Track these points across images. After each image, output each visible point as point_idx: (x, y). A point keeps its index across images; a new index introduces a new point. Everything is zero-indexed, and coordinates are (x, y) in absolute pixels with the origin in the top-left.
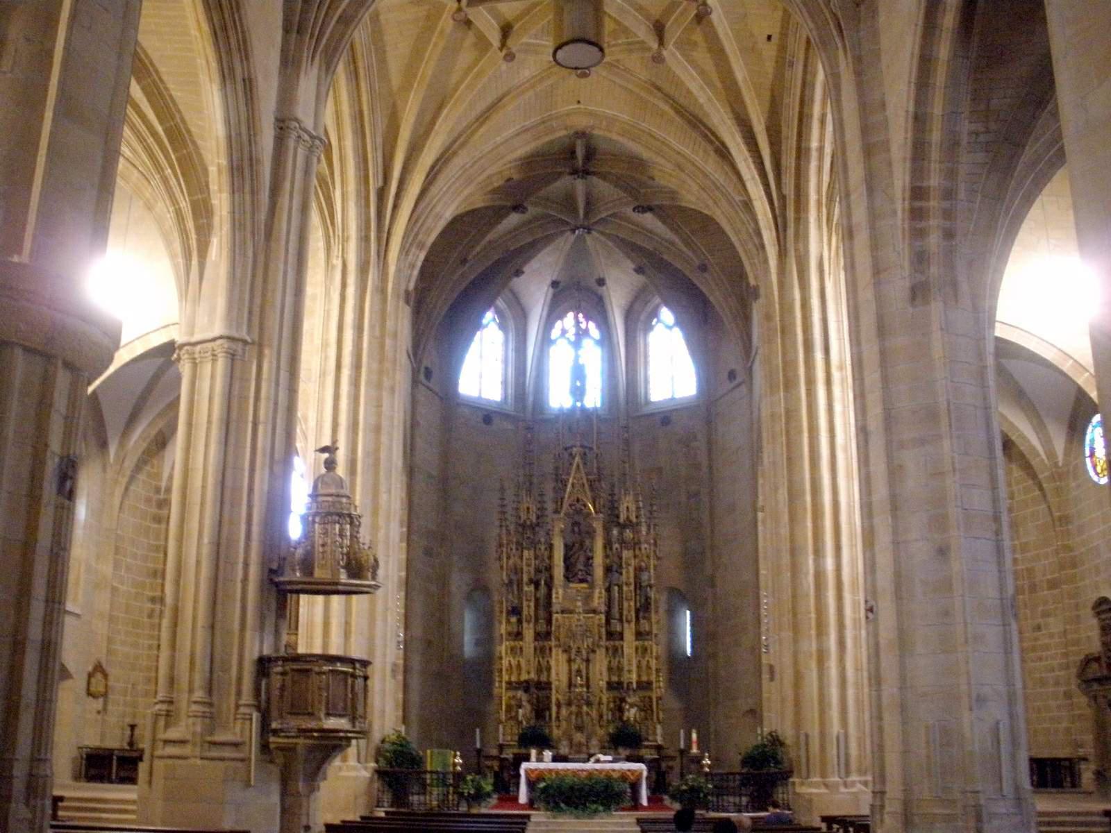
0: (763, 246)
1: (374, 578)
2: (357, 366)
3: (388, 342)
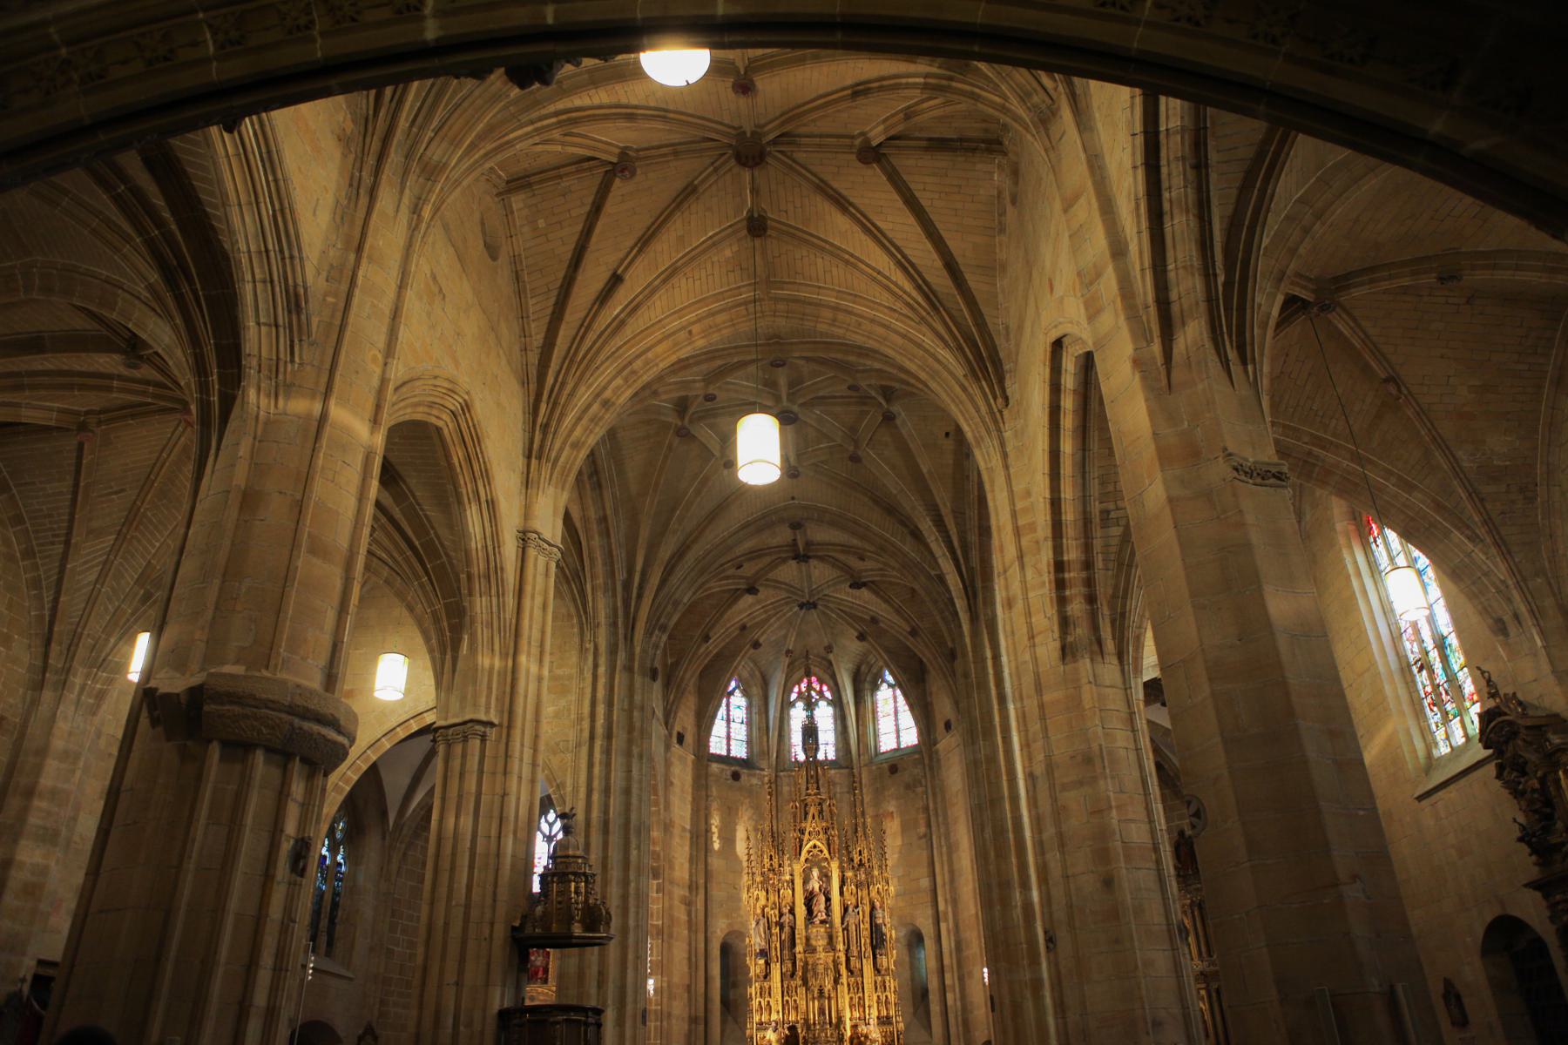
0: (956, 614)
1: (607, 931)
2: (609, 736)
3: (636, 714)
